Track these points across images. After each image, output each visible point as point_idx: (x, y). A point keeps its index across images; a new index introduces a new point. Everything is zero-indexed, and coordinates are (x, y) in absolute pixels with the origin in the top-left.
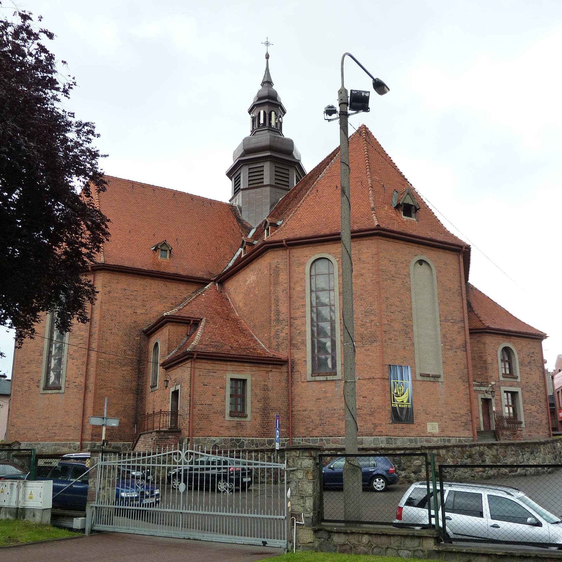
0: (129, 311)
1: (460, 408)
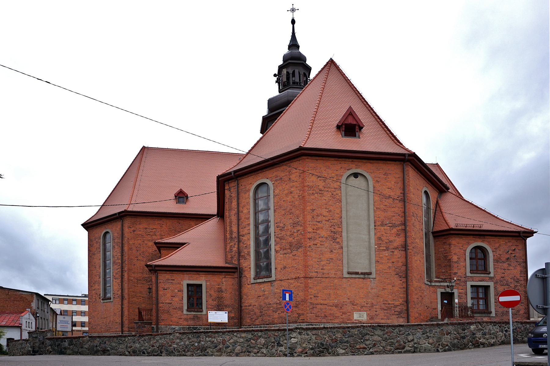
1: (394, 300)
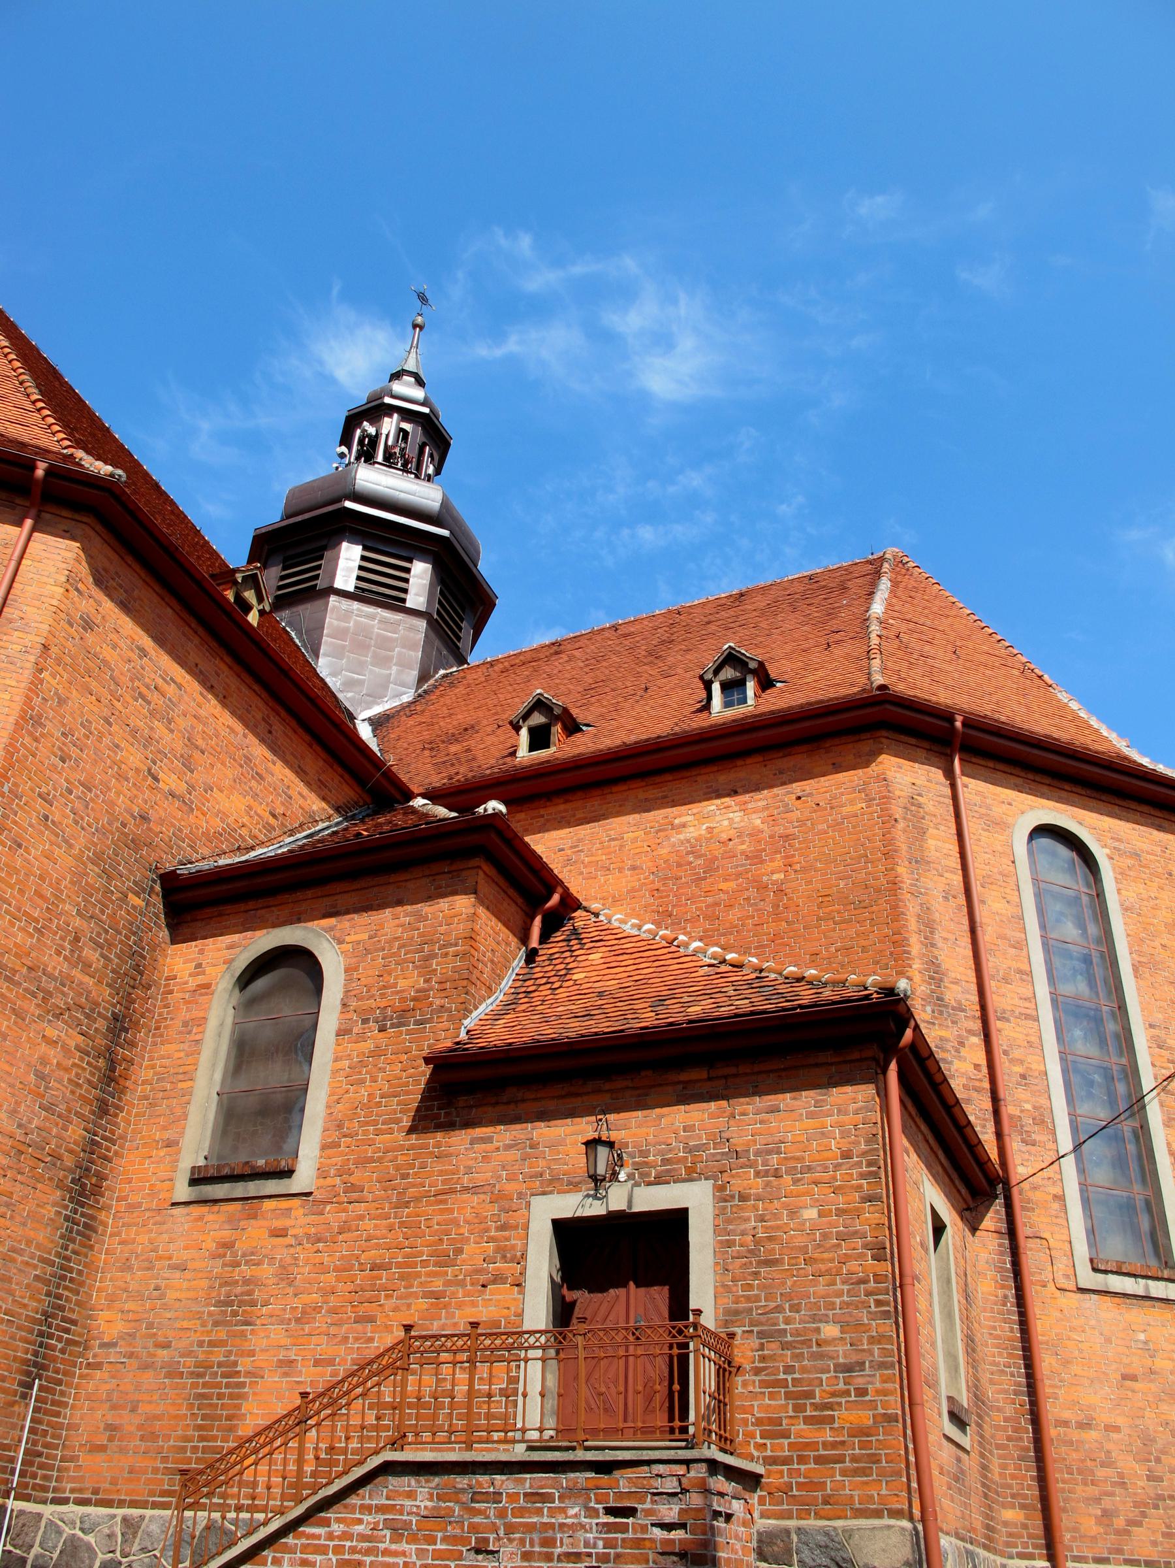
0: (134, 757)
